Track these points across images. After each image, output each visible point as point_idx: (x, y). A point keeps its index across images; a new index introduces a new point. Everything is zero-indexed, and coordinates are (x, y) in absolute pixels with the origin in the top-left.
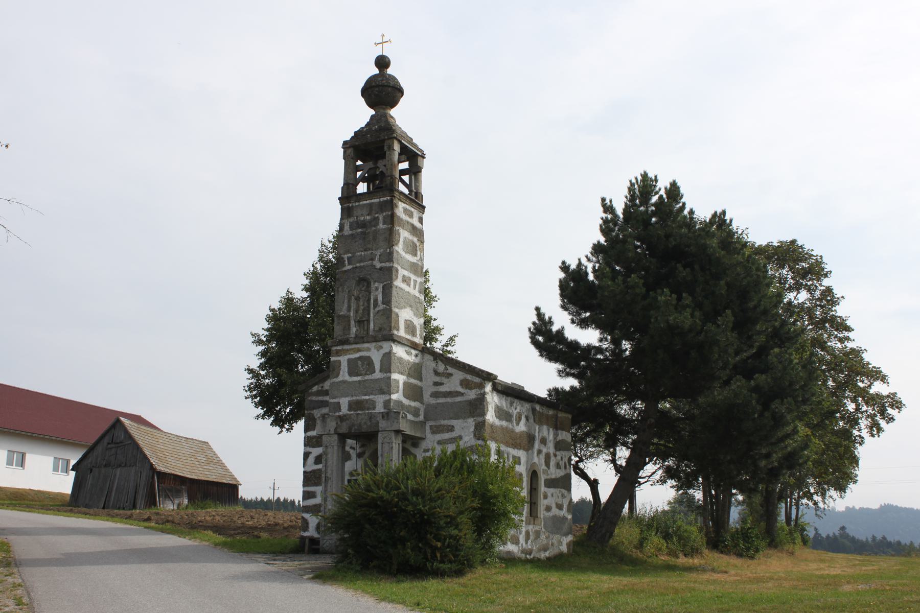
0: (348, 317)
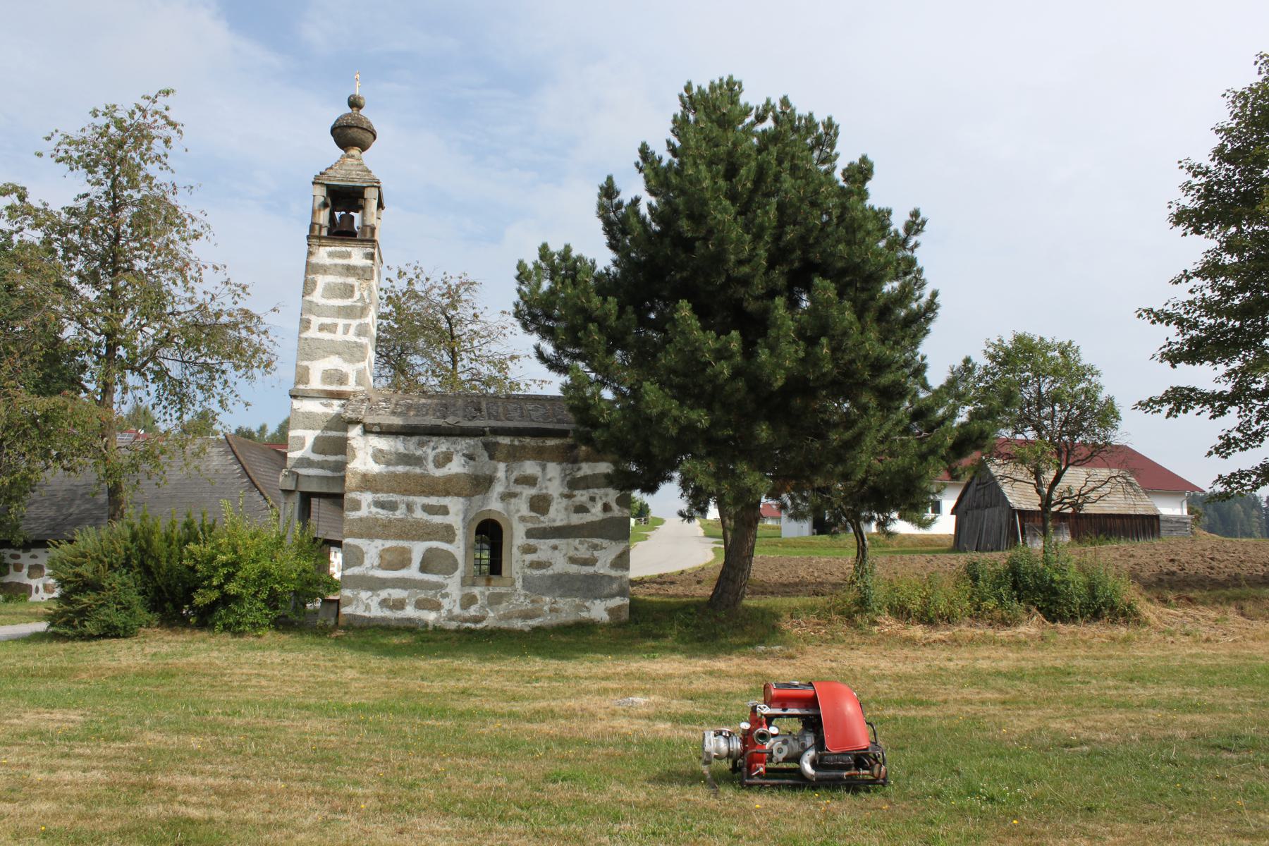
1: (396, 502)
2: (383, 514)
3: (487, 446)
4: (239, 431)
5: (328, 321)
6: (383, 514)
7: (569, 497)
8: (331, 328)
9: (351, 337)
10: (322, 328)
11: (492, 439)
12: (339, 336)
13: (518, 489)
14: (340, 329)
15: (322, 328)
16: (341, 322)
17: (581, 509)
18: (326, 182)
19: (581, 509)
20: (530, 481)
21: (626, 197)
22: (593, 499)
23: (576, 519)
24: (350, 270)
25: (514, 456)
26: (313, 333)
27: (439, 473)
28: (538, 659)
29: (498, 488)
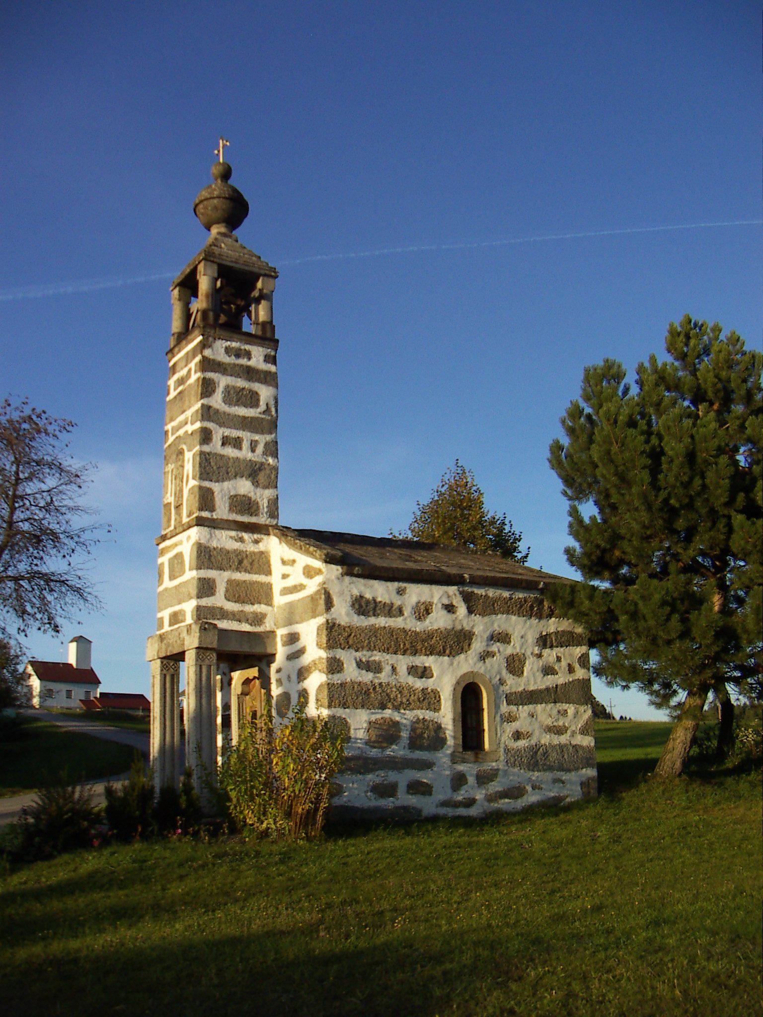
0: (170, 503)
1: (380, 662)
2: (367, 677)
3: (468, 598)
4: (573, 565)
5: (235, 433)
6: (367, 677)
7: (540, 656)
8: (237, 443)
9: (258, 456)
10: (225, 441)
11: (468, 589)
12: (245, 453)
13: (494, 648)
14: (246, 445)
15: (225, 441)
16: (246, 436)
17: (548, 671)
18: (218, 261)
19: (548, 671)
20: (503, 638)
21: (675, 326)
22: (559, 659)
23: (550, 681)
24: (250, 373)
25: (489, 608)
26: (216, 446)
27: (419, 627)
28: (86, 855)
29: (478, 646)
